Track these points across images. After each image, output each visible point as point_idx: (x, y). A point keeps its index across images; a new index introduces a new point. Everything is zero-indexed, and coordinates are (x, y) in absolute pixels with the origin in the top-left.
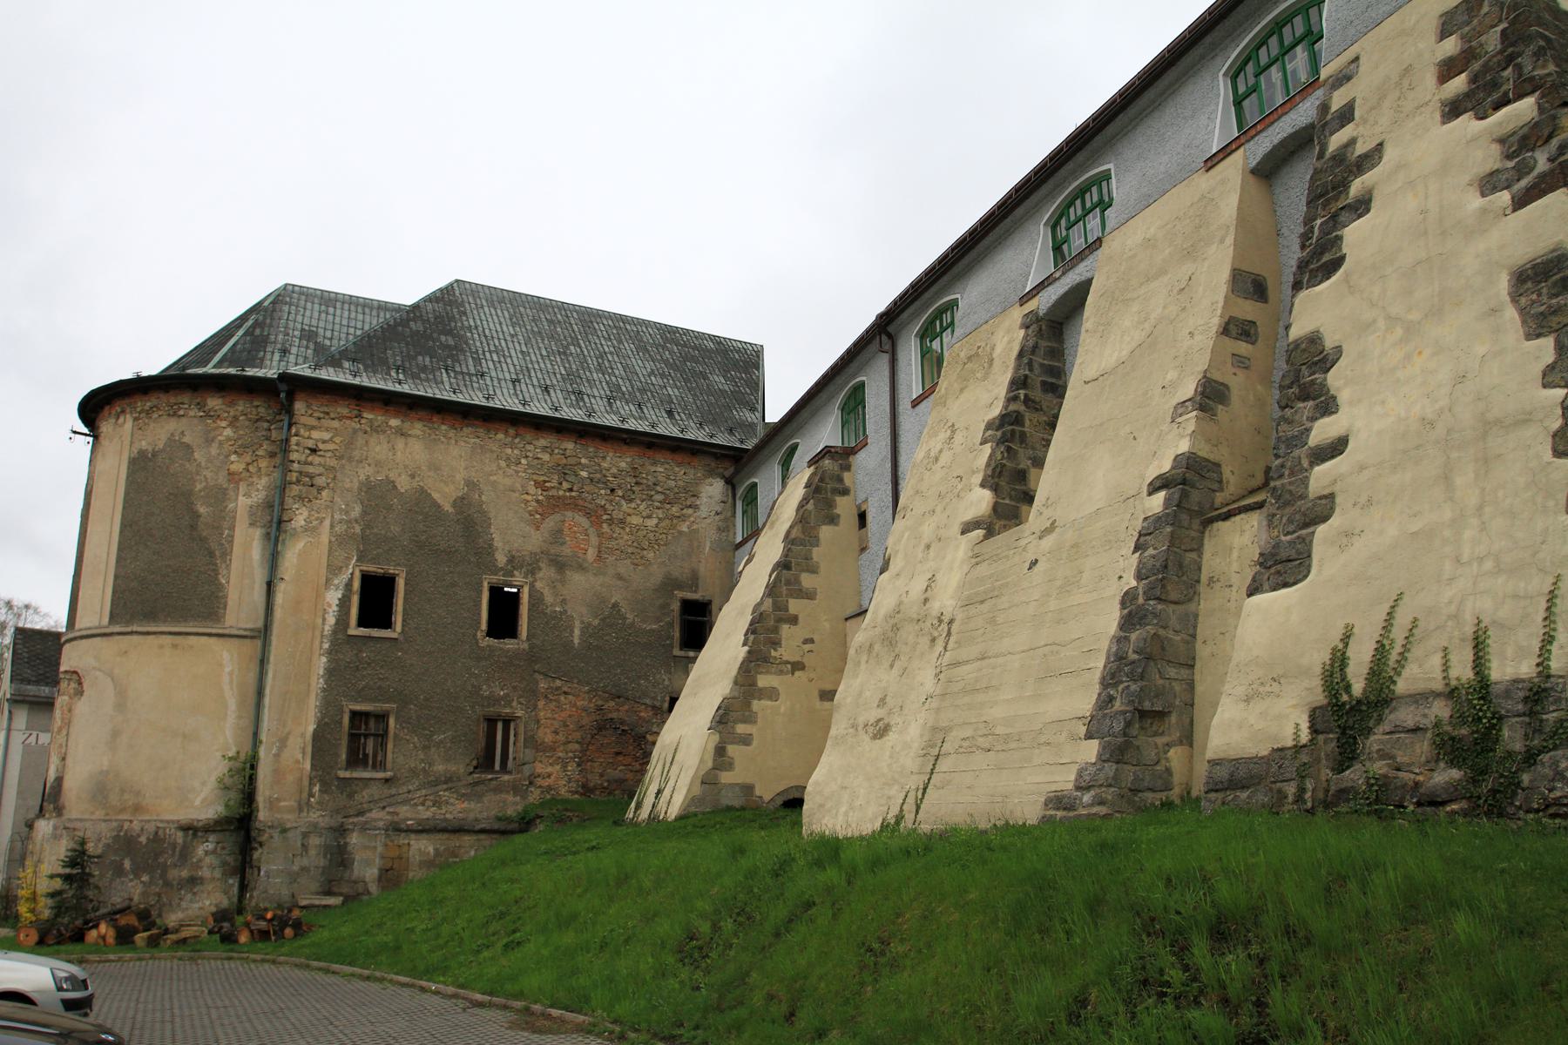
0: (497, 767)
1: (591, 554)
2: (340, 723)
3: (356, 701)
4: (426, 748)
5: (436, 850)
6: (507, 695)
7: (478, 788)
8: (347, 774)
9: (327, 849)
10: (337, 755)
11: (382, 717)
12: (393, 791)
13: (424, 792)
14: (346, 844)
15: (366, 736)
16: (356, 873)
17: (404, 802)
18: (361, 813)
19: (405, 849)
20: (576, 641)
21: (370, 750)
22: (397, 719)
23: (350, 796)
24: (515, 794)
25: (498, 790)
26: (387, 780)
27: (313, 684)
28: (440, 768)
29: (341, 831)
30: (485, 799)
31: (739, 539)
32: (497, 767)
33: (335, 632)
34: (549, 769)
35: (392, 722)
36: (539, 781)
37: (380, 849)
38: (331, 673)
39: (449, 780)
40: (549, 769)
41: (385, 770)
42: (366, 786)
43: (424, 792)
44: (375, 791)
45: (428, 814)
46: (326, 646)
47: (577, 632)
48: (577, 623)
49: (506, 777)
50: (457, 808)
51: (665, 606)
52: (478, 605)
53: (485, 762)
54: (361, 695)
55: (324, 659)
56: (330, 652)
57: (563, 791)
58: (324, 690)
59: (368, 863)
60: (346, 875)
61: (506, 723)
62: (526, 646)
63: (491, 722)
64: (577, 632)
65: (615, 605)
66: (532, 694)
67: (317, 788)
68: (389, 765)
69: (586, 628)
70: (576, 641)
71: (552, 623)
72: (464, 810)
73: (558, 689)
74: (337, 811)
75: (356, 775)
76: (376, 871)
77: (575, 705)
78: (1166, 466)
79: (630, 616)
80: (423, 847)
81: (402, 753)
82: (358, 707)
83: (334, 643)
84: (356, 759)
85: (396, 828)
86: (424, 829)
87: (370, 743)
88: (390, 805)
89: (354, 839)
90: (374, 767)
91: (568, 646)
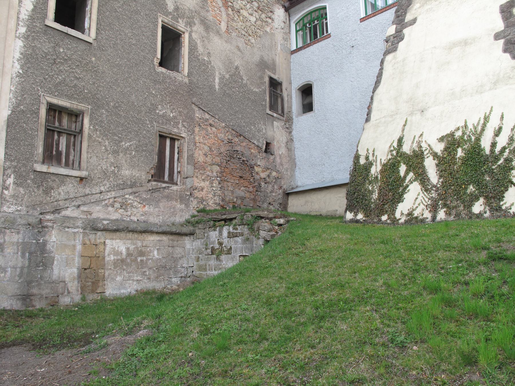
0: (166, 178)
1: (223, 26)
2: (37, 113)
3: (52, 94)
4: (115, 152)
5: (128, 249)
6: (175, 117)
7: (156, 195)
8: (44, 168)
9: (24, 247)
10: (33, 146)
11: (75, 115)
12: (87, 191)
13: (113, 194)
14: (45, 244)
15: (60, 133)
16: (56, 272)
17: (97, 202)
18: (57, 211)
19: (101, 247)
20: (217, 87)
21: (63, 147)
22: (91, 121)
23: (47, 192)
24: (181, 203)
25: (169, 198)
26: (82, 179)
27: (8, 65)
28: (126, 172)
29: (40, 227)
30: (161, 204)
31: (294, 48)
32: (166, 178)
33: (32, 18)
34: (202, 184)
35: (86, 121)
36: (196, 193)
37: (79, 247)
38: (29, 59)
39: (133, 184)
40: (202, 184)
41: (80, 168)
42: (63, 183)
43: (113, 194)
44: (69, 188)
45: (115, 216)
46: (23, 30)
47: (217, 80)
48: (217, 74)
49: (175, 188)
50: (138, 213)
51: (261, 78)
52: (155, 36)
53: (158, 174)
54: (57, 89)
55: (20, 43)
56: (26, 37)
57: (211, 203)
58: (19, 75)
59: (68, 263)
60: (46, 275)
61: (173, 140)
62: (186, 80)
63: (162, 137)
64: (217, 80)
65: (237, 68)
66: (190, 119)
67: (10, 181)
68: (84, 164)
69: (222, 78)
70: (217, 87)
71: (200, 66)
72: (145, 214)
73: (207, 120)
74: (34, 207)
75: (53, 169)
76: (75, 270)
77: (216, 136)
78: (345, 206)
79: (245, 78)
80: (117, 246)
81: (94, 154)
82: (55, 101)
83: (30, 28)
84: (51, 155)
85: (93, 227)
86: (116, 229)
87: (63, 141)
88: (84, 204)
89: (53, 238)
90: (67, 165)
91: (212, 87)
